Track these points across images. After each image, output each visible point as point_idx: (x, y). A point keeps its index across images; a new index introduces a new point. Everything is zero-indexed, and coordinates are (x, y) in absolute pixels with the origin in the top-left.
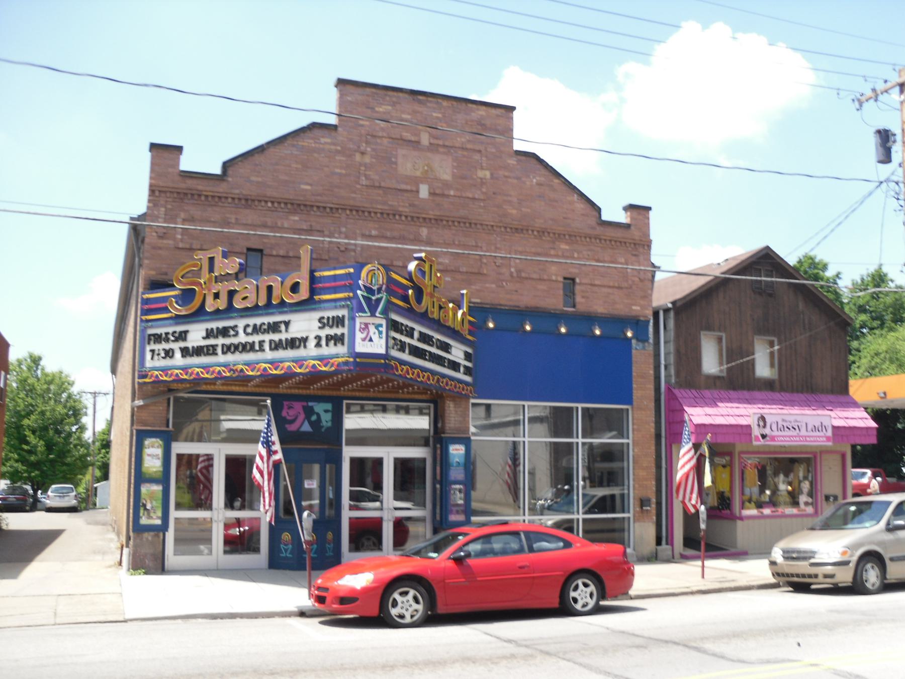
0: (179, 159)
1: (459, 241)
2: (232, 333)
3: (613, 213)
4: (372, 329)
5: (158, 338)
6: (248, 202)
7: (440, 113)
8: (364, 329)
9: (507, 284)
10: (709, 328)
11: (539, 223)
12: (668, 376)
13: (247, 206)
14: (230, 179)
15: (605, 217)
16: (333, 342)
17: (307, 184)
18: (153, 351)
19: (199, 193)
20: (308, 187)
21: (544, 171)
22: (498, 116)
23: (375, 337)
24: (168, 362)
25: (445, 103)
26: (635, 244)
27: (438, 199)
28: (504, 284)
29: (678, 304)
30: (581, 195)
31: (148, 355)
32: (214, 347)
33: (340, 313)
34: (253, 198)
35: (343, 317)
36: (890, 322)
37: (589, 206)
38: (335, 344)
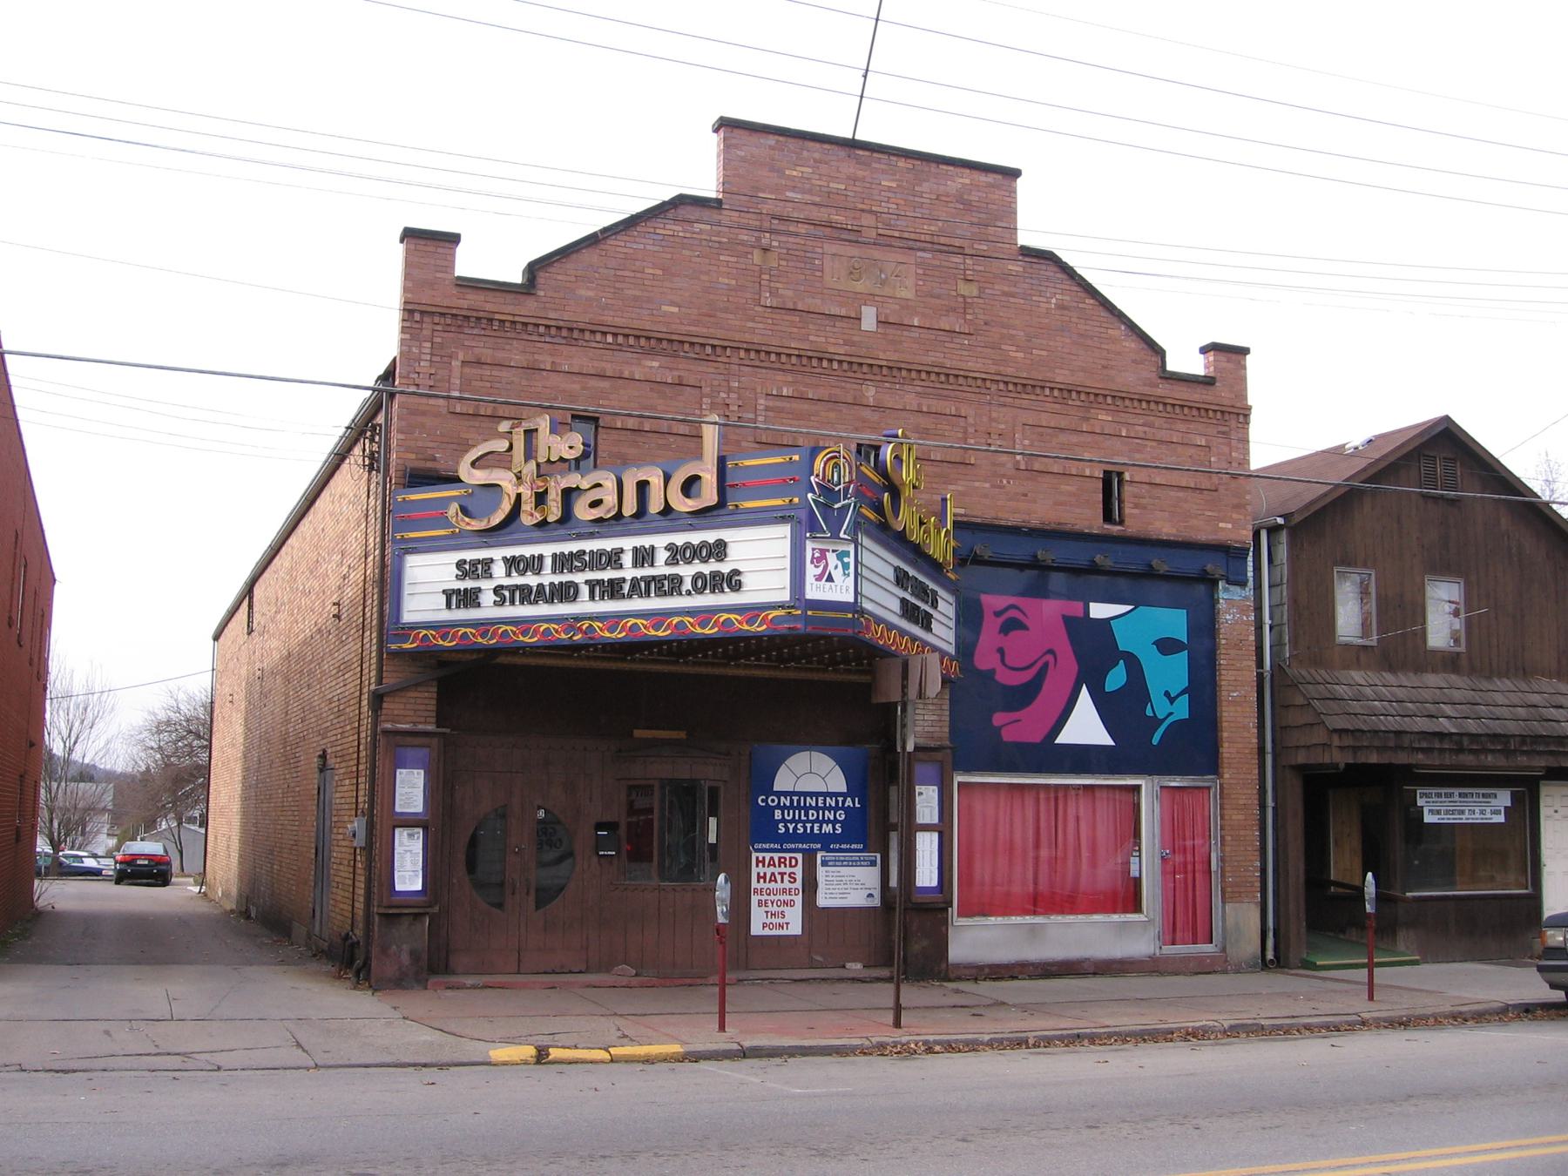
0: (453, 255)
1: (929, 406)
3: (1185, 359)
4: (832, 558)
6: (571, 333)
7: (893, 180)
8: (819, 560)
9: (1009, 483)
10: (1347, 561)
11: (1062, 376)
12: (1277, 645)
13: (571, 342)
14: (541, 293)
15: (1172, 366)
17: (672, 304)
19: (491, 316)
20: (675, 310)
21: (1068, 284)
22: (990, 186)
23: (837, 575)
25: (902, 163)
26: (1223, 412)
27: (891, 331)
28: (1005, 482)
29: (1297, 519)
30: (1133, 328)
34: (582, 326)
36: (1247, 589)
37: (1143, 345)
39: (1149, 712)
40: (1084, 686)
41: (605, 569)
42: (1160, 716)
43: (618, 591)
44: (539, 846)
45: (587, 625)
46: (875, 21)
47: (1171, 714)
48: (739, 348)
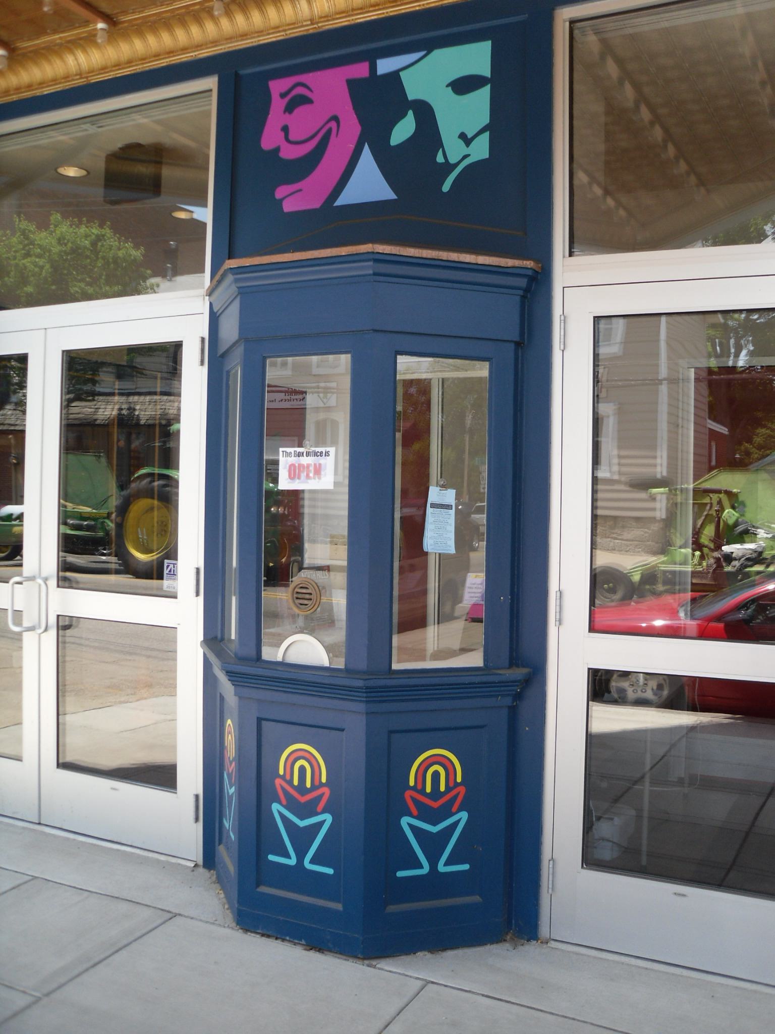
39: (440, 159)
40: (366, 145)
42: (452, 160)
44: (155, 288)
46: (203, 297)
47: (468, 155)
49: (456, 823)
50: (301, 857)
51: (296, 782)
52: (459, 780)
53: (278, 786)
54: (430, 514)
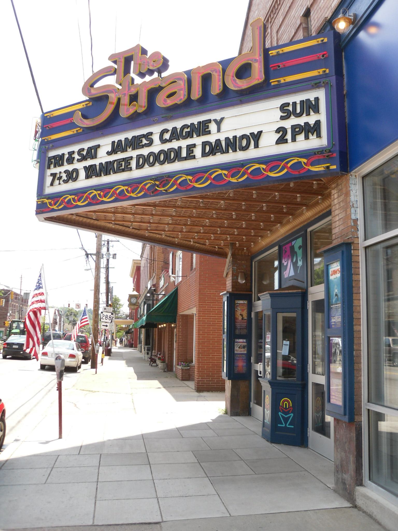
2: (144, 141)
5: (59, 160)
16: (303, 135)
18: (54, 175)
24: (71, 186)
31: (49, 180)
32: (128, 160)
33: (311, 95)
35: (317, 99)
38: (307, 138)
41: (174, 161)
43: (139, 144)
45: (149, 185)
48: (211, 226)
49: (281, 415)
50: (286, 424)
51: (284, 407)
52: (291, 406)
53: (280, 408)
54: (123, 61)
